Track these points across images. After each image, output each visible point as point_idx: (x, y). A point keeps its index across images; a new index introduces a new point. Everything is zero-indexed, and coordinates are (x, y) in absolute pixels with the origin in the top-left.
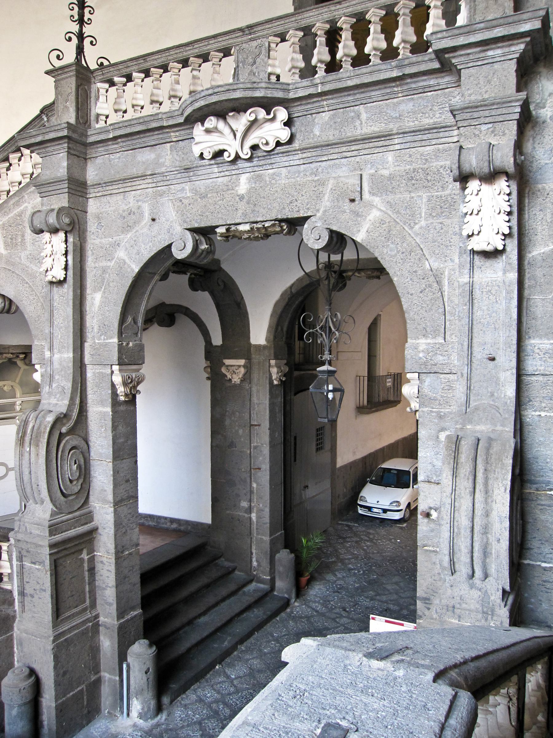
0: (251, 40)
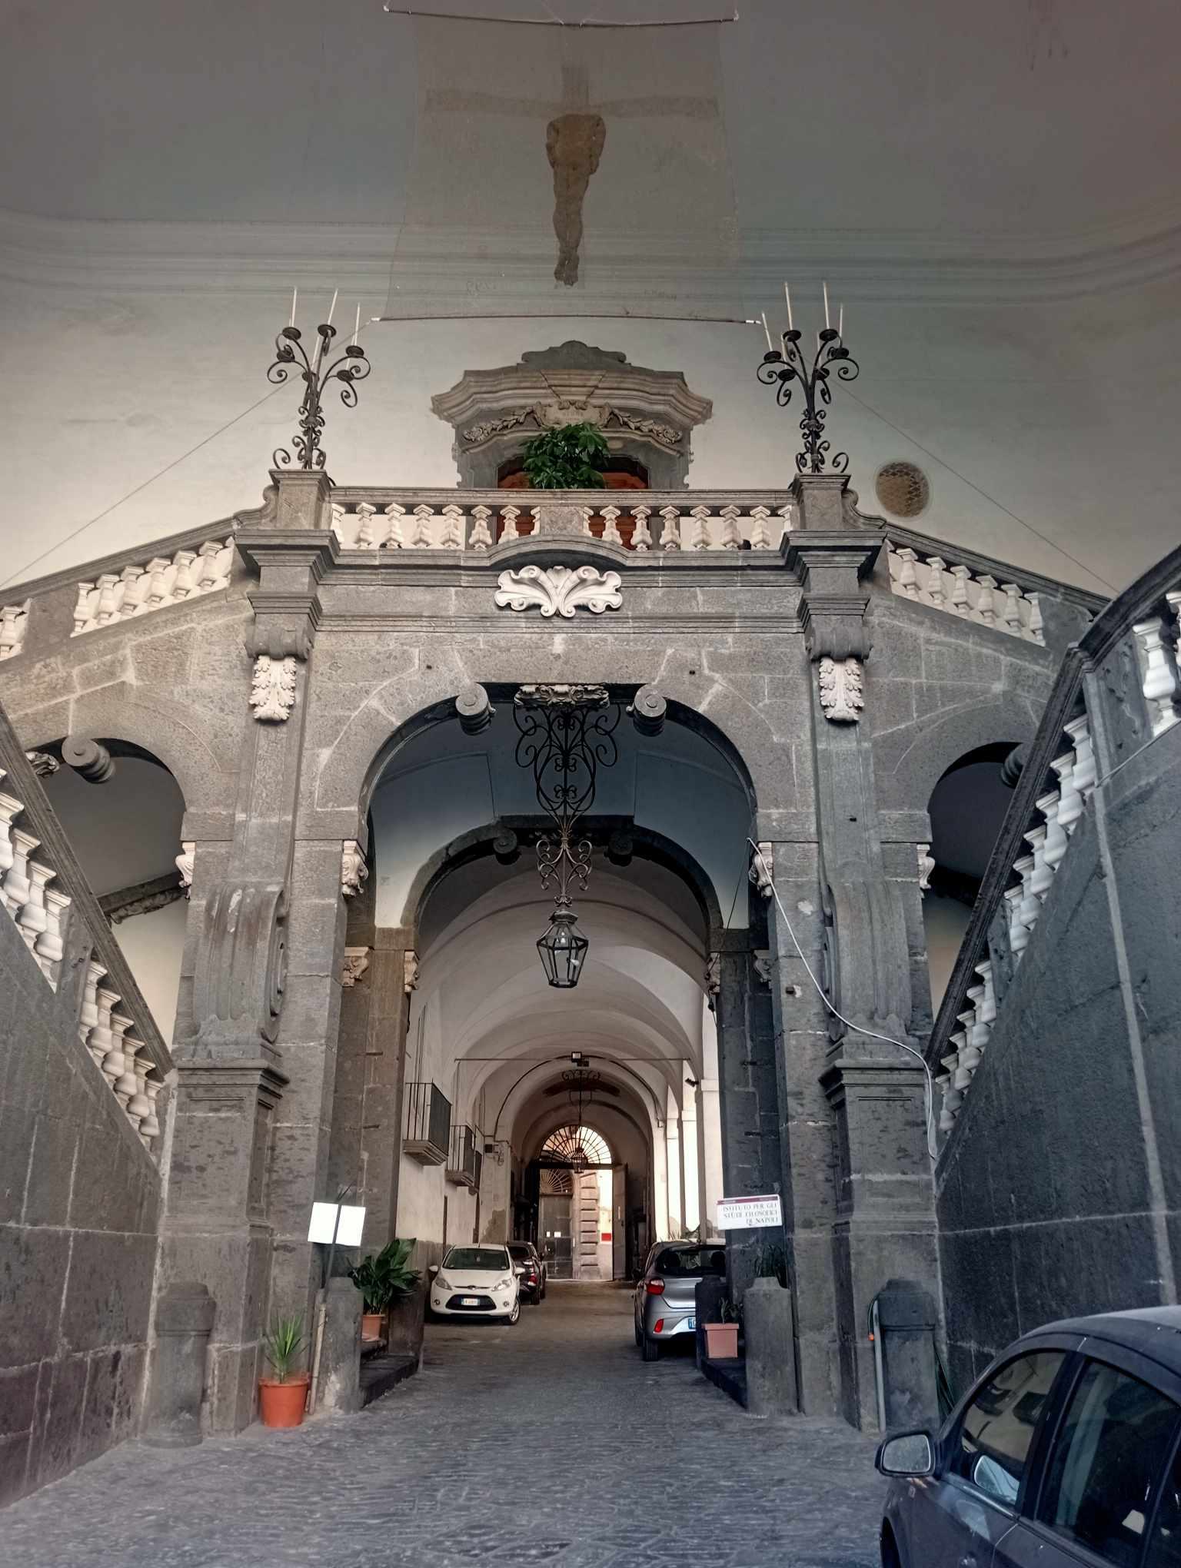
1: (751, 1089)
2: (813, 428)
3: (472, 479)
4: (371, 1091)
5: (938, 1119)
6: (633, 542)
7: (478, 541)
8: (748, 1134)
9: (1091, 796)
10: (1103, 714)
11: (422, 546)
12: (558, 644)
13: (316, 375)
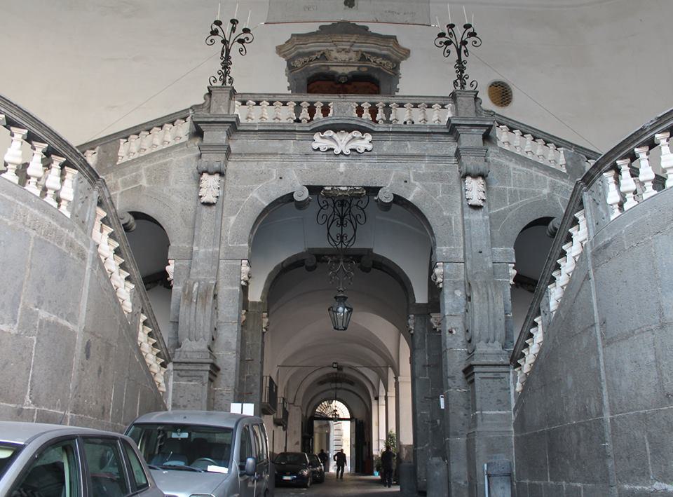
0: (343, 102)
1: (428, 378)
2: (460, 66)
3: (295, 88)
4: (248, 377)
5: (515, 387)
6: (377, 119)
7: (303, 118)
8: (426, 398)
9: (585, 244)
10: (591, 210)
11: (277, 121)
12: (342, 167)
13: (228, 42)
